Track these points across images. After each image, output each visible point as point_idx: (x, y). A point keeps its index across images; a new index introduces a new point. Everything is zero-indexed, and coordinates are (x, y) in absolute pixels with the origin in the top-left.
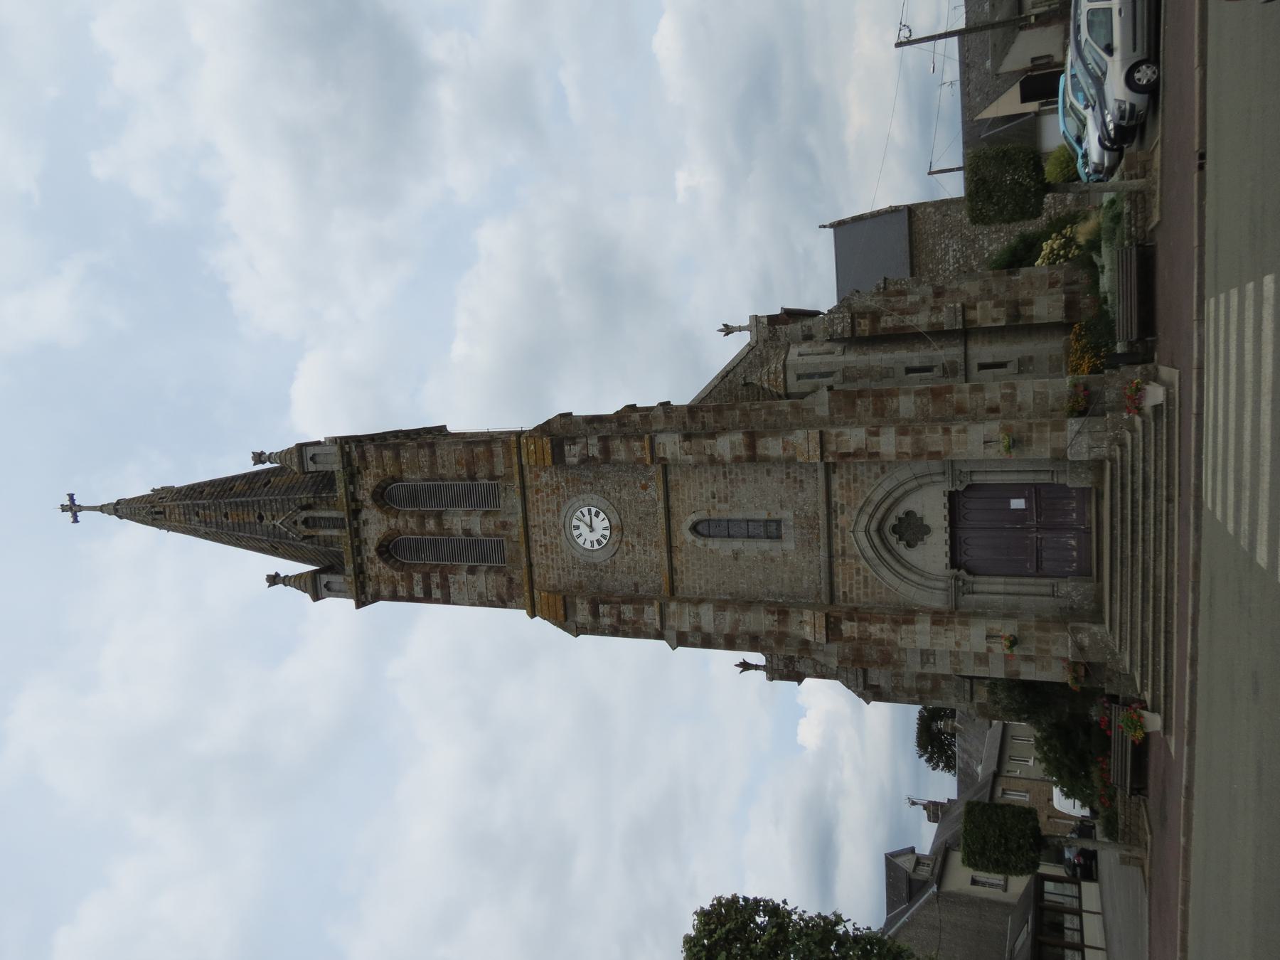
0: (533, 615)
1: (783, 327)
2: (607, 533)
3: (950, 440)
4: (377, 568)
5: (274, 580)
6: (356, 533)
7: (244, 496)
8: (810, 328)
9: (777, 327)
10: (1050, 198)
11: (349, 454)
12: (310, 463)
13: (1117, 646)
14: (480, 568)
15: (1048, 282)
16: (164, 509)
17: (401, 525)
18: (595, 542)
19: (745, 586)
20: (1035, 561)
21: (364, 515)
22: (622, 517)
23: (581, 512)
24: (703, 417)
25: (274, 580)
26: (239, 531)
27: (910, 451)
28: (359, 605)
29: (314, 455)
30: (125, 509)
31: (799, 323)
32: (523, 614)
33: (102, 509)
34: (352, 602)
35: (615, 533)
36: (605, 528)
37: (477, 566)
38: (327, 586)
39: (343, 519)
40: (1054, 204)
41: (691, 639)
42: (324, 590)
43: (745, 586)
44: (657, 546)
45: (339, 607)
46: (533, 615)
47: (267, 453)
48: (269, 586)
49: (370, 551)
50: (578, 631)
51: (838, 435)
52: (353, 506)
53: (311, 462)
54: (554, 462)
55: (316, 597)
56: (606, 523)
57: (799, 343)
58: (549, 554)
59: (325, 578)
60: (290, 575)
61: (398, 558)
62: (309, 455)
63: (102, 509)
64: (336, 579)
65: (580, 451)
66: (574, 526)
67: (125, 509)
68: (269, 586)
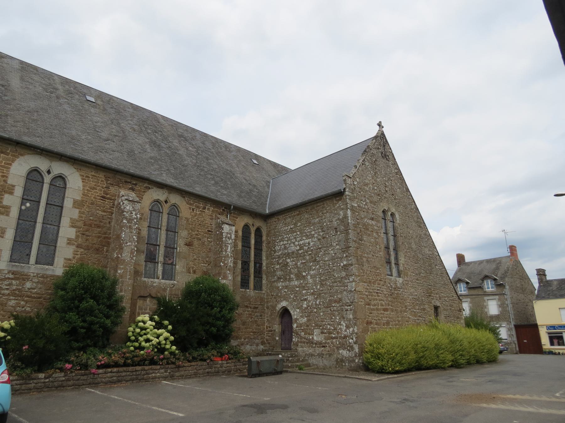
10: (346, 333)
40: (341, 337)
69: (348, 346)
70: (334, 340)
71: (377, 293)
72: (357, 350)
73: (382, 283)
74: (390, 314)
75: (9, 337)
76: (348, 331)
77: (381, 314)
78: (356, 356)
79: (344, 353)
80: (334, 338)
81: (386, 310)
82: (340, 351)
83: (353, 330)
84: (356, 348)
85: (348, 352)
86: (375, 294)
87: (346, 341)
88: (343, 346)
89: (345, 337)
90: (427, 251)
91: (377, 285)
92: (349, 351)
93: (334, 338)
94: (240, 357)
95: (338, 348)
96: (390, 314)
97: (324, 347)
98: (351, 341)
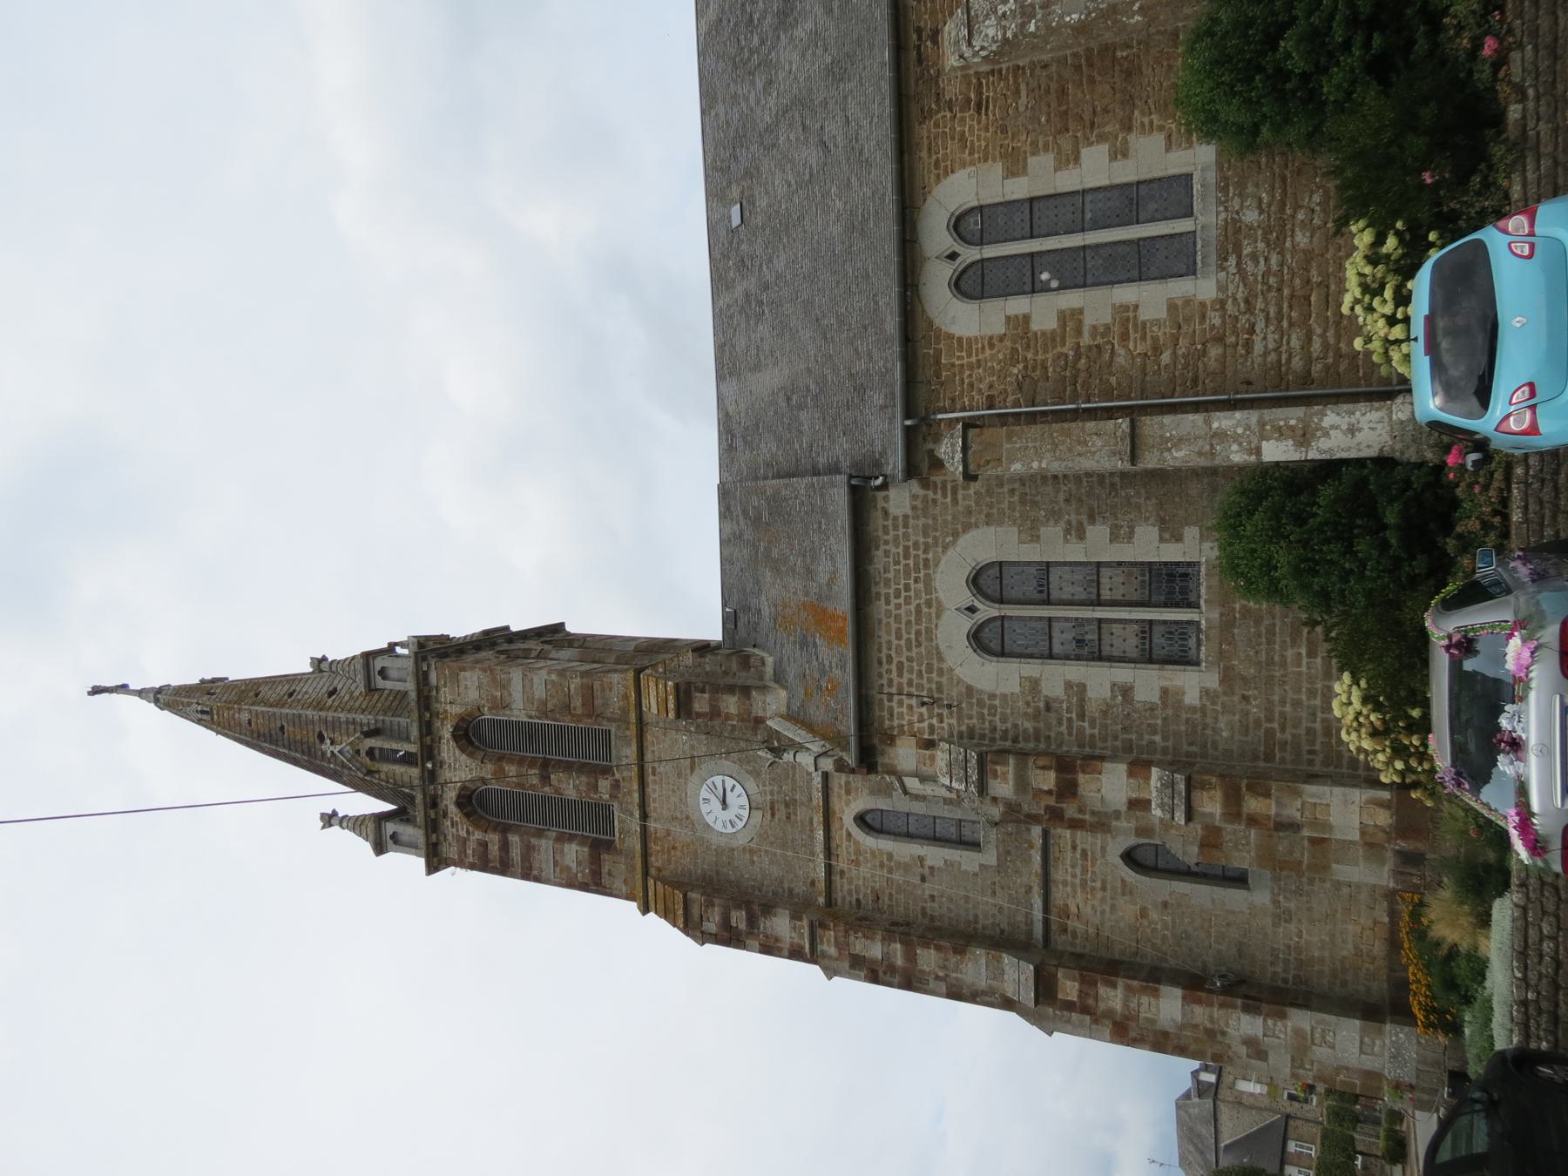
0: (645, 910)
2: (745, 813)
4: (455, 825)
5: (329, 819)
6: (432, 776)
7: (276, 706)
12: (379, 678)
13: (806, 935)
14: (549, 833)
16: (211, 709)
18: (728, 823)
23: (723, 781)
25: (329, 819)
26: (296, 751)
28: (432, 868)
29: (383, 668)
30: (170, 699)
32: (632, 906)
33: (141, 693)
34: (420, 863)
35: (758, 815)
36: (742, 807)
37: (544, 830)
38: (394, 837)
39: (416, 754)
41: (932, 984)
42: (390, 842)
45: (407, 865)
46: (645, 910)
47: (330, 660)
48: (323, 827)
49: (450, 797)
50: (703, 937)
53: (380, 678)
54: (678, 716)
55: (380, 849)
56: (744, 801)
59: (390, 827)
60: (350, 815)
62: (378, 668)
63: (141, 693)
64: (407, 831)
66: (704, 799)
67: (170, 699)
68: (323, 827)
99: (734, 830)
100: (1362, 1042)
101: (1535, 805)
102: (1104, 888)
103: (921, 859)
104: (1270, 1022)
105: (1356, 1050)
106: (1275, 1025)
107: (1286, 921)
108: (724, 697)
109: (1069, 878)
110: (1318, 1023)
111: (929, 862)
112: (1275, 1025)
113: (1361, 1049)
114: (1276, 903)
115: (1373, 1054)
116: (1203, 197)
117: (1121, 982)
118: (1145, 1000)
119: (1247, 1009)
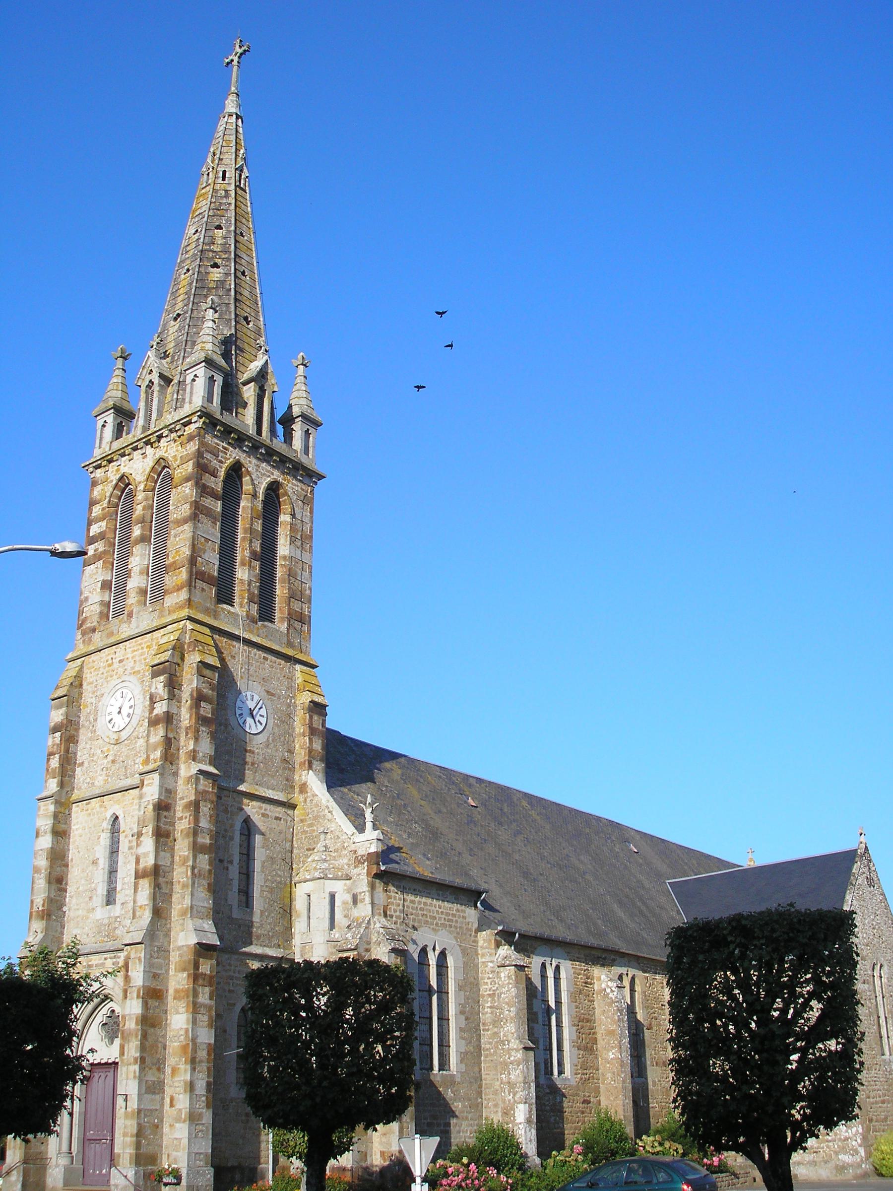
1: (365, 871)
3: (130, 1064)
8: (363, 900)
9: (366, 863)
10: (847, 1134)
11: (190, 423)
15: (384, 1150)
17: (139, 498)
19: (76, 874)
20: (94, 1138)
21: (149, 450)
22: (126, 742)
24: (186, 818)
27: (126, 1028)
31: (367, 889)
40: (840, 1139)
43: (76, 874)
44: (106, 781)
51: (140, 959)
52: (153, 439)
57: (349, 890)
58: (107, 669)
61: (123, 498)
65: (158, 694)
69: (850, 1150)
70: (831, 1144)
71: (875, 1081)
72: (863, 1154)
73: (878, 1067)
74: (887, 1107)
75: (755, 1018)
76: (850, 1131)
77: (880, 1107)
78: (862, 1160)
79: (846, 1158)
80: (830, 1141)
81: (883, 1102)
82: (840, 1157)
83: (857, 1130)
84: (862, 1151)
85: (851, 1157)
86: (873, 1083)
87: (848, 1145)
88: (843, 1150)
89: (846, 1139)
90: (442, 1102)
91: (873, 1072)
92: (853, 1155)
93: (830, 1141)
94: (91, 935)
95: (836, 1153)
96: (887, 1107)
97: (816, 1152)
98: (854, 1143)
99: (237, 716)
100: (201, 1153)
101: (640, 1017)
102: (230, 991)
103: (231, 862)
104: (204, 1098)
105: (196, 1151)
106: (203, 1102)
107: (224, 1106)
108: (320, 741)
109: (233, 968)
110: (207, 1128)
111: (230, 867)
112: (203, 1102)
113: (197, 1153)
114: (232, 1100)
115: (195, 1160)
116: (639, 1006)
117: (213, 1003)
118: (206, 1018)
119: (208, 1084)
